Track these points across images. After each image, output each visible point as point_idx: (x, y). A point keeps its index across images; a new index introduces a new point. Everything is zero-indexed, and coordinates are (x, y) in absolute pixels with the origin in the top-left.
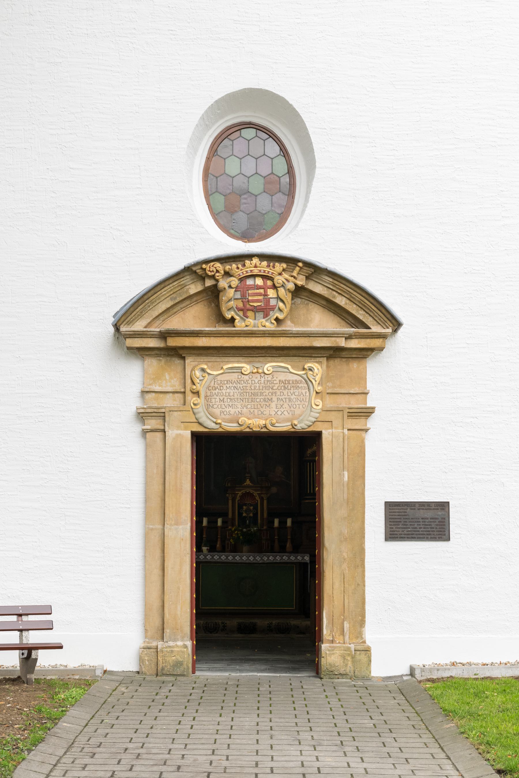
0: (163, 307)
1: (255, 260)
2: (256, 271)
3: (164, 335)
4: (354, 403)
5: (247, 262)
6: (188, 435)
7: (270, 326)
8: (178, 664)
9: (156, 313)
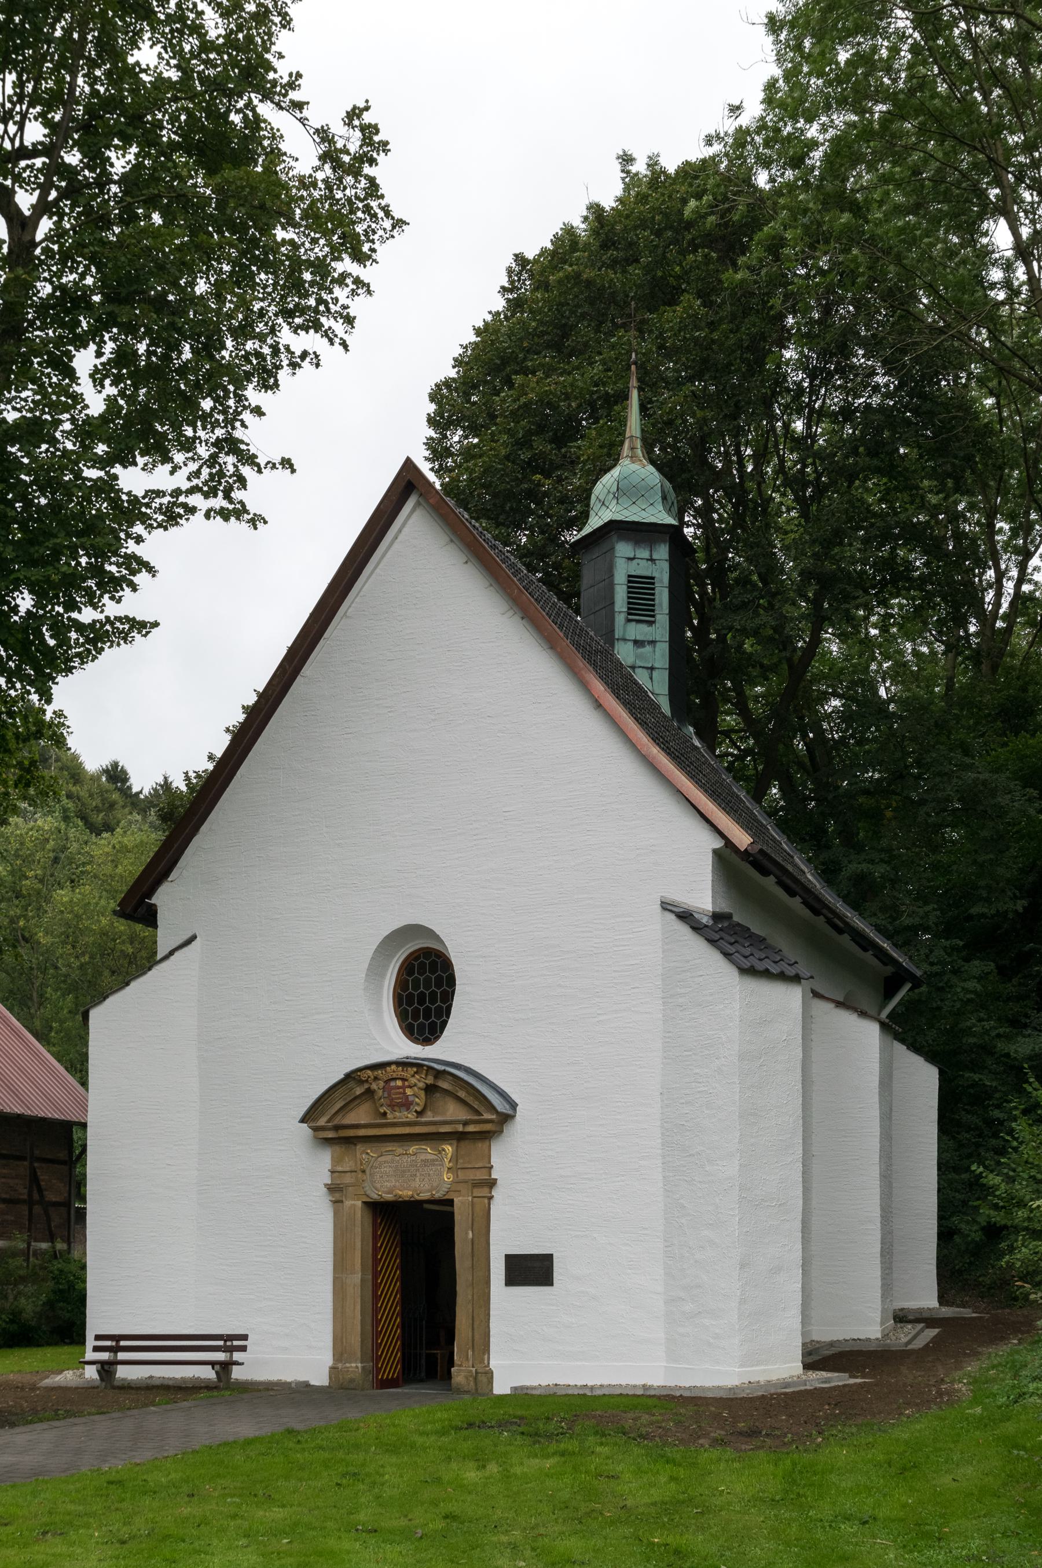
0: (338, 1106)
1: (393, 1067)
2: (395, 1076)
3: (337, 1128)
4: (481, 1175)
5: (388, 1069)
6: (359, 1203)
7: (411, 1116)
8: (352, 1381)
9: (333, 1111)
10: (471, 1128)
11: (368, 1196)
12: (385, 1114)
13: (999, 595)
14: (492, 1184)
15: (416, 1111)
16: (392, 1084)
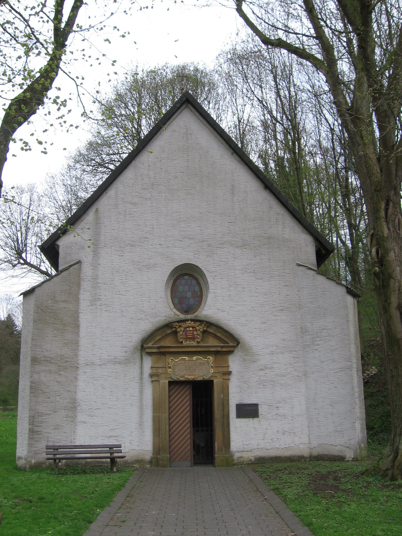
0: (157, 338)
1: (189, 322)
4: (224, 370)
7: (195, 344)
10: (224, 350)
11: (172, 378)
12: (182, 342)
13: (398, 138)
14: (230, 373)
15: (197, 342)
16: (188, 329)
